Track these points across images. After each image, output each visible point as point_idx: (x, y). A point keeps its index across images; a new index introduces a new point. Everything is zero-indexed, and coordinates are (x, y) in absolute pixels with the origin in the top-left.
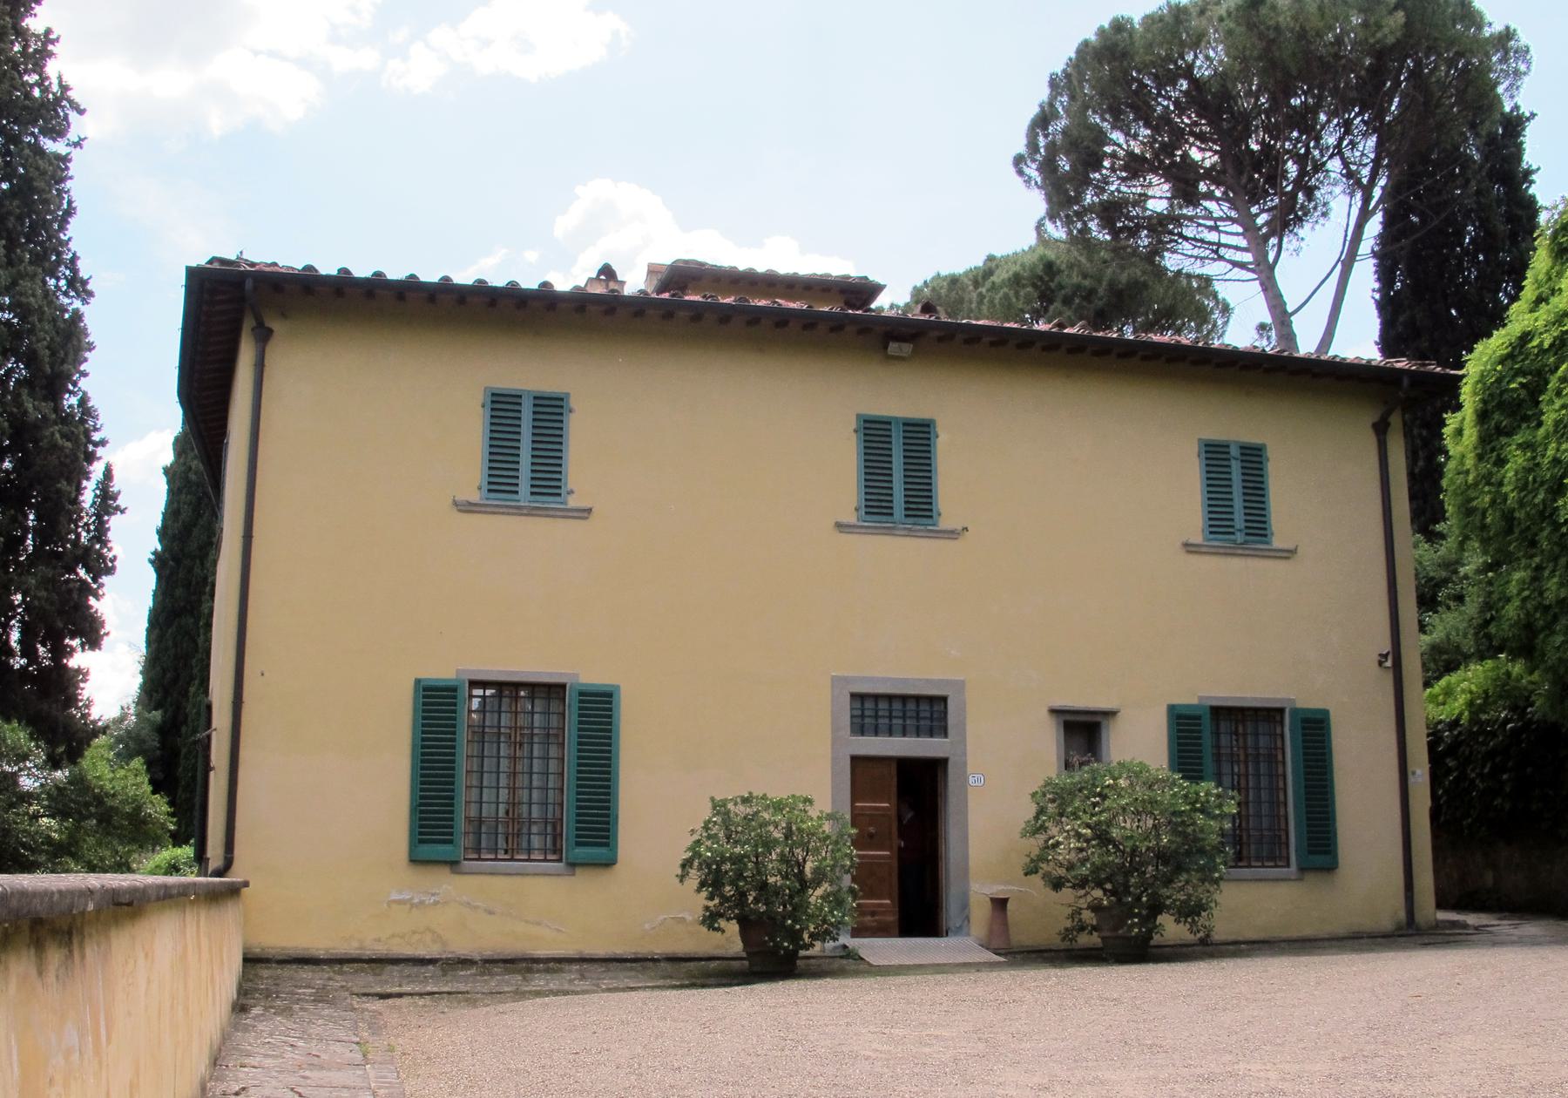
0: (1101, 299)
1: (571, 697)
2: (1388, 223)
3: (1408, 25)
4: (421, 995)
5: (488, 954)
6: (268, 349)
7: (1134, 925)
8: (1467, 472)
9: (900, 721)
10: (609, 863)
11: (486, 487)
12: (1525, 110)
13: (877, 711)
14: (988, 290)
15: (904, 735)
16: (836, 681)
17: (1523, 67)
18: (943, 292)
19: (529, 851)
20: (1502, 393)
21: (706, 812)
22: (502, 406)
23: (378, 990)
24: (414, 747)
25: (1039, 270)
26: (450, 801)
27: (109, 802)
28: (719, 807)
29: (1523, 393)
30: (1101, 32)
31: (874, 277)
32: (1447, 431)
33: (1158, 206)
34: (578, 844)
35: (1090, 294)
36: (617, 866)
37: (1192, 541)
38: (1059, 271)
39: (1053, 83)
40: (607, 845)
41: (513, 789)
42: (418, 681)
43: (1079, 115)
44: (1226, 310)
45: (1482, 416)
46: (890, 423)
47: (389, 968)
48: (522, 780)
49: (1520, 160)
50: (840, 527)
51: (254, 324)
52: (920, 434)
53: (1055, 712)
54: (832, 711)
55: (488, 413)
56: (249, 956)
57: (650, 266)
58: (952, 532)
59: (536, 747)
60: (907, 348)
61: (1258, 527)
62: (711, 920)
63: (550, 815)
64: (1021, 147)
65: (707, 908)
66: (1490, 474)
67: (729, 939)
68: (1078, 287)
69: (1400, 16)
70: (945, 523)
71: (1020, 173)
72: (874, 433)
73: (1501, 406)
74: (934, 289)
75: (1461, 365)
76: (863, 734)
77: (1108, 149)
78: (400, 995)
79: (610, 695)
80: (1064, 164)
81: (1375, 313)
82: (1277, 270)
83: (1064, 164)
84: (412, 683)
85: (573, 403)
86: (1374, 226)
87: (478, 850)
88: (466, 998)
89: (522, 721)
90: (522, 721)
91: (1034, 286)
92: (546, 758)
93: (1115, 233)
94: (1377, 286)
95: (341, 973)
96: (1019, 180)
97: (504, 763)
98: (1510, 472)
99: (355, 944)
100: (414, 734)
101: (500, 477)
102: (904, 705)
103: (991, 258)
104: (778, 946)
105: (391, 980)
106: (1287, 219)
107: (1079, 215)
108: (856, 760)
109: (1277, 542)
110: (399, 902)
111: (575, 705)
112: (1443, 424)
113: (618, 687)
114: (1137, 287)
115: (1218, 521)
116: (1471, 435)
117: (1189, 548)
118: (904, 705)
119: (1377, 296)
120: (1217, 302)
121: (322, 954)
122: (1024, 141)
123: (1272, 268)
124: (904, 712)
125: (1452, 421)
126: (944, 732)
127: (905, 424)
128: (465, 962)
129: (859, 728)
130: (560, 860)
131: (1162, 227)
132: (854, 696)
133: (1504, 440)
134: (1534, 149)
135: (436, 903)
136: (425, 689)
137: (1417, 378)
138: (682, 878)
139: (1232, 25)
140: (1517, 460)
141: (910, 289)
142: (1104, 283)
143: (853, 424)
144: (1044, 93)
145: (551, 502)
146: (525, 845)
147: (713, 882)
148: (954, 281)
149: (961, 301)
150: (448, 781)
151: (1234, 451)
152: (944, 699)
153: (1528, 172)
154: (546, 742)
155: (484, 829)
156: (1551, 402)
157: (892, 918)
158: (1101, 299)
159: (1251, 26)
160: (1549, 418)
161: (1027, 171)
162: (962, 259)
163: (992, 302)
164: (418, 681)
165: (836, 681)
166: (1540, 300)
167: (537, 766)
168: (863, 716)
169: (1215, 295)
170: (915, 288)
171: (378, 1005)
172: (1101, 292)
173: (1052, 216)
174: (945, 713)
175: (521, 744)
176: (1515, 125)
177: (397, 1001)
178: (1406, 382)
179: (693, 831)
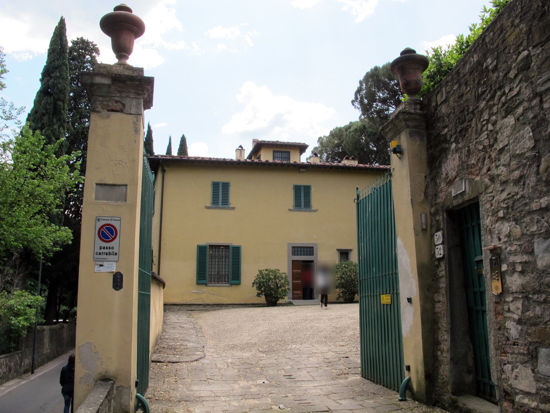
0: (378, 135)
1: (231, 249)
4: (199, 310)
5: (213, 303)
6: (165, 174)
7: (347, 295)
9: (300, 252)
10: (239, 284)
11: (212, 203)
13: (298, 250)
14: (348, 133)
15: (301, 255)
16: (288, 244)
18: (338, 132)
19: (222, 282)
21: (258, 273)
22: (215, 185)
23: (190, 309)
25: (362, 127)
26: (205, 271)
28: (260, 272)
30: (372, 70)
31: (307, 143)
34: (232, 280)
35: (375, 134)
36: (241, 284)
40: (239, 280)
41: (218, 268)
42: (198, 245)
46: (300, 186)
47: (192, 306)
48: (221, 266)
50: (290, 210)
51: (162, 169)
53: (338, 250)
54: (73, 303)
55: (212, 187)
57: (253, 140)
58: (315, 210)
59: (223, 259)
60: (304, 170)
62: (259, 295)
63: (226, 274)
64: (353, 98)
65: (258, 293)
67: (263, 299)
68: (372, 132)
70: (313, 209)
71: (353, 105)
72: (297, 189)
74: (335, 132)
76: (295, 255)
78: (195, 310)
79: (239, 248)
80: (366, 101)
83: (366, 101)
84: (196, 246)
87: (211, 281)
88: (208, 310)
89: (220, 253)
90: (220, 253)
92: (226, 262)
95: (182, 307)
96: (353, 107)
97: (217, 263)
99: (185, 302)
102: (304, 249)
103: (351, 123)
104: (272, 300)
105: (193, 308)
108: (293, 261)
110: (195, 293)
111: (232, 250)
113: (241, 246)
118: (304, 249)
121: (178, 304)
124: (301, 250)
126: (313, 255)
127: (304, 187)
128: (209, 305)
129: (294, 254)
130: (229, 283)
132: (293, 247)
135: (202, 293)
136: (200, 247)
138: (253, 286)
143: (293, 187)
145: (226, 206)
146: (221, 280)
147: (259, 288)
150: (205, 266)
152: (313, 247)
154: (225, 258)
155: (212, 277)
157: (301, 296)
158: (378, 135)
163: (349, 136)
164: (198, 245)
165: (288, 244)
167: (224, 263)
168: (295, 252)
170: (331, 131)
171: (190, 312)
174: (313, 250)
175: (220, 259)
177: (194, 311)
179: (255, 277)
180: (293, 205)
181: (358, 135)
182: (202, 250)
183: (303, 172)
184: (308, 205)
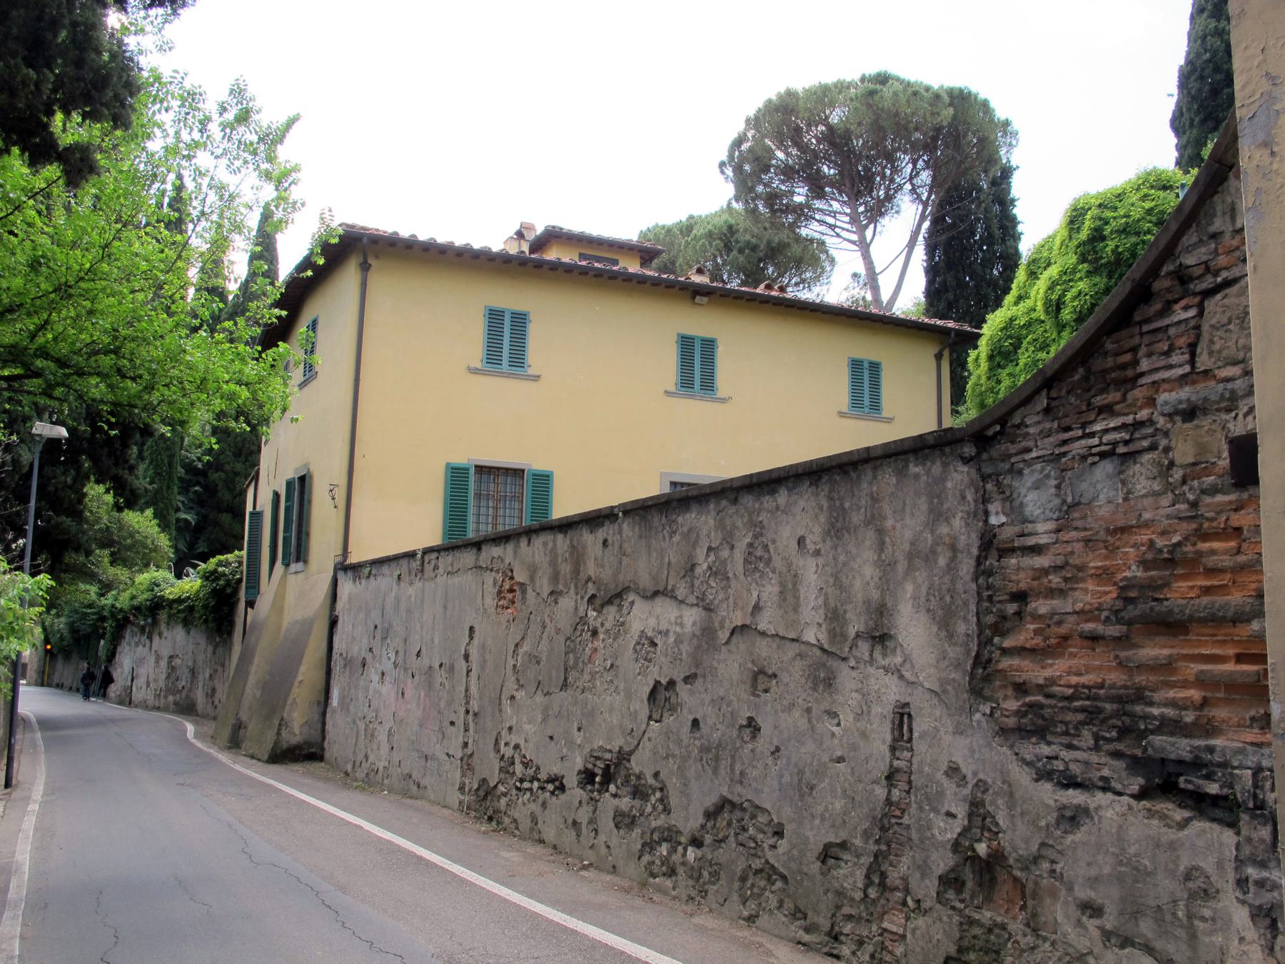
2: (932, 223)
3: (954, 117)
8: (982, 385)
12: (1013, 164)
16: (662, 474)
17: (1014, 143)
20: (1000, 347)
24: (445, 499)
25: (725, 230)
27: (138, 537)
29: (1011, 348)
30: (780, 96)
32: (970, 359)
33: (799, 199)
35: (754, 248)
37: (843, 410)
38: (737, 231)
39: (748, 121)
42: (448, 464)
43: (758, 141)
44: (832, 261)
45: (991, 358)
49: (1009, 193)
50: (667, 392)
51: (361, 260)
52: (709, 346)
55: (487, 320)
56: (39, 681)
60: (705, 299)
61: (876, 406)
64: (724, 156)
66: (993, 388)
68: (748, 242)
69: (951, 111)
70: (720, 394)
71: (722, 172)
73: (1000, 353)
74: (655, 234)
75: (981, 328)
77: (774, 162)
81: (923, 274)
82: (872, 248)
85: (532, 317)
86: (926, 224)
91: (720, 239)
93: (773, 211)
94: (925, 258)
96: (722, 177)
98: (1003, 386)
100: (445, 492)
101: (493, 356)
106: (877, 211)
107: (753, 200)
109: (885, 414)
112: (968, 355)
113: (552, 472)
114: (783, 246)
115: (856, 401)
116: (984, 365)
117: (842, 414)
119: (925, 264)
120: (828, 256)
122: (726, 153)
123: (868, 246)
125: (973, 354)
131: (802, 213)
133: (1000, 370)
134: (1018, 187)
137: (959, 333)
139: (858, 105)
140: (1006, 382)
141: (638, 232)
142: (764, 242)
144: (741, 127)
145: (518, 371)
148: (669, 231)
149: (672, 243)
151: (866, 365)
153: (1013, 201)
156: (1023, 354)
159: (869, 106)
160: (1022, 362)
161: (726, 171)
162: (671, 214)
163: (694, 247)
165: (662, 474)
166: (1020, 298)
169: (827, 252)
172: (762, 247)
173: (737, 199)
176: (1007, 172)
178: (953, 334)
180: (674, 381)
181: (717, 245)
182: (456, 476)
183: (701, 305)
184: (708, 384)
